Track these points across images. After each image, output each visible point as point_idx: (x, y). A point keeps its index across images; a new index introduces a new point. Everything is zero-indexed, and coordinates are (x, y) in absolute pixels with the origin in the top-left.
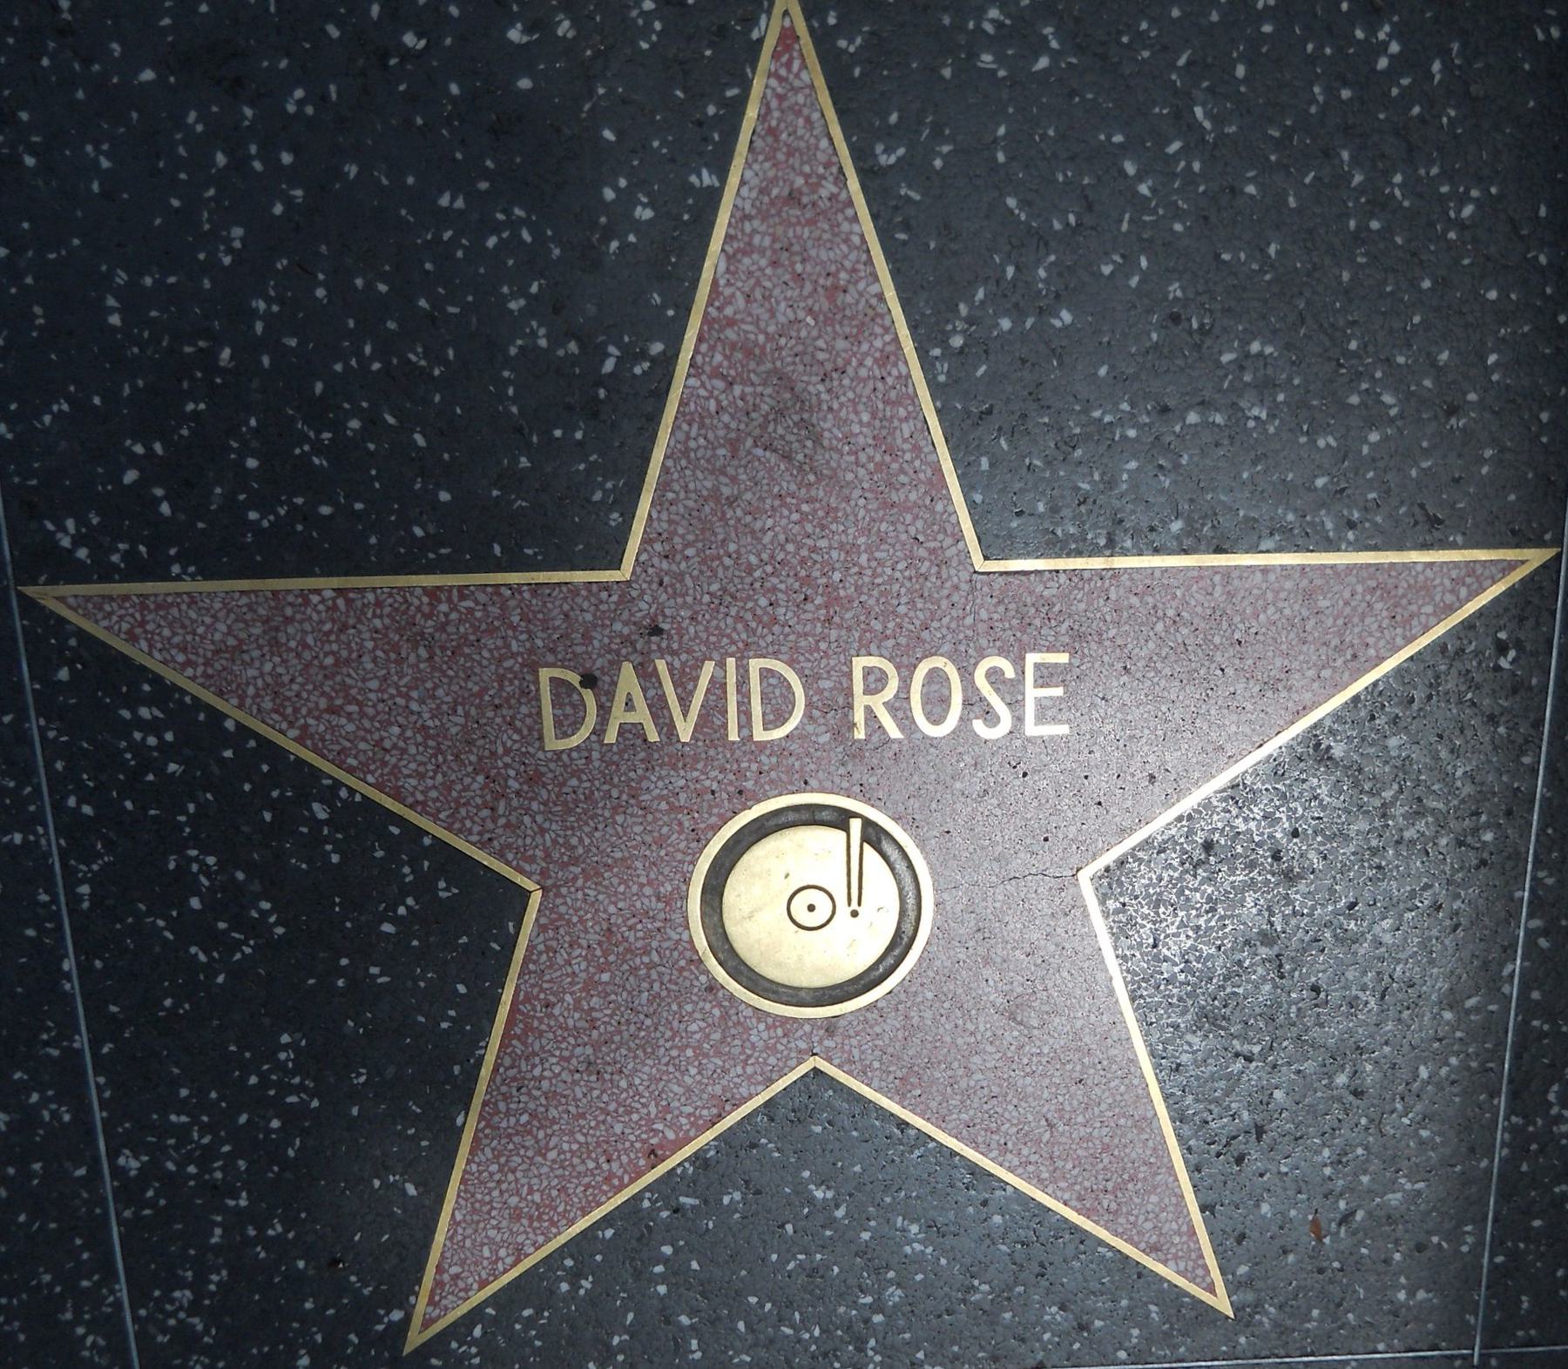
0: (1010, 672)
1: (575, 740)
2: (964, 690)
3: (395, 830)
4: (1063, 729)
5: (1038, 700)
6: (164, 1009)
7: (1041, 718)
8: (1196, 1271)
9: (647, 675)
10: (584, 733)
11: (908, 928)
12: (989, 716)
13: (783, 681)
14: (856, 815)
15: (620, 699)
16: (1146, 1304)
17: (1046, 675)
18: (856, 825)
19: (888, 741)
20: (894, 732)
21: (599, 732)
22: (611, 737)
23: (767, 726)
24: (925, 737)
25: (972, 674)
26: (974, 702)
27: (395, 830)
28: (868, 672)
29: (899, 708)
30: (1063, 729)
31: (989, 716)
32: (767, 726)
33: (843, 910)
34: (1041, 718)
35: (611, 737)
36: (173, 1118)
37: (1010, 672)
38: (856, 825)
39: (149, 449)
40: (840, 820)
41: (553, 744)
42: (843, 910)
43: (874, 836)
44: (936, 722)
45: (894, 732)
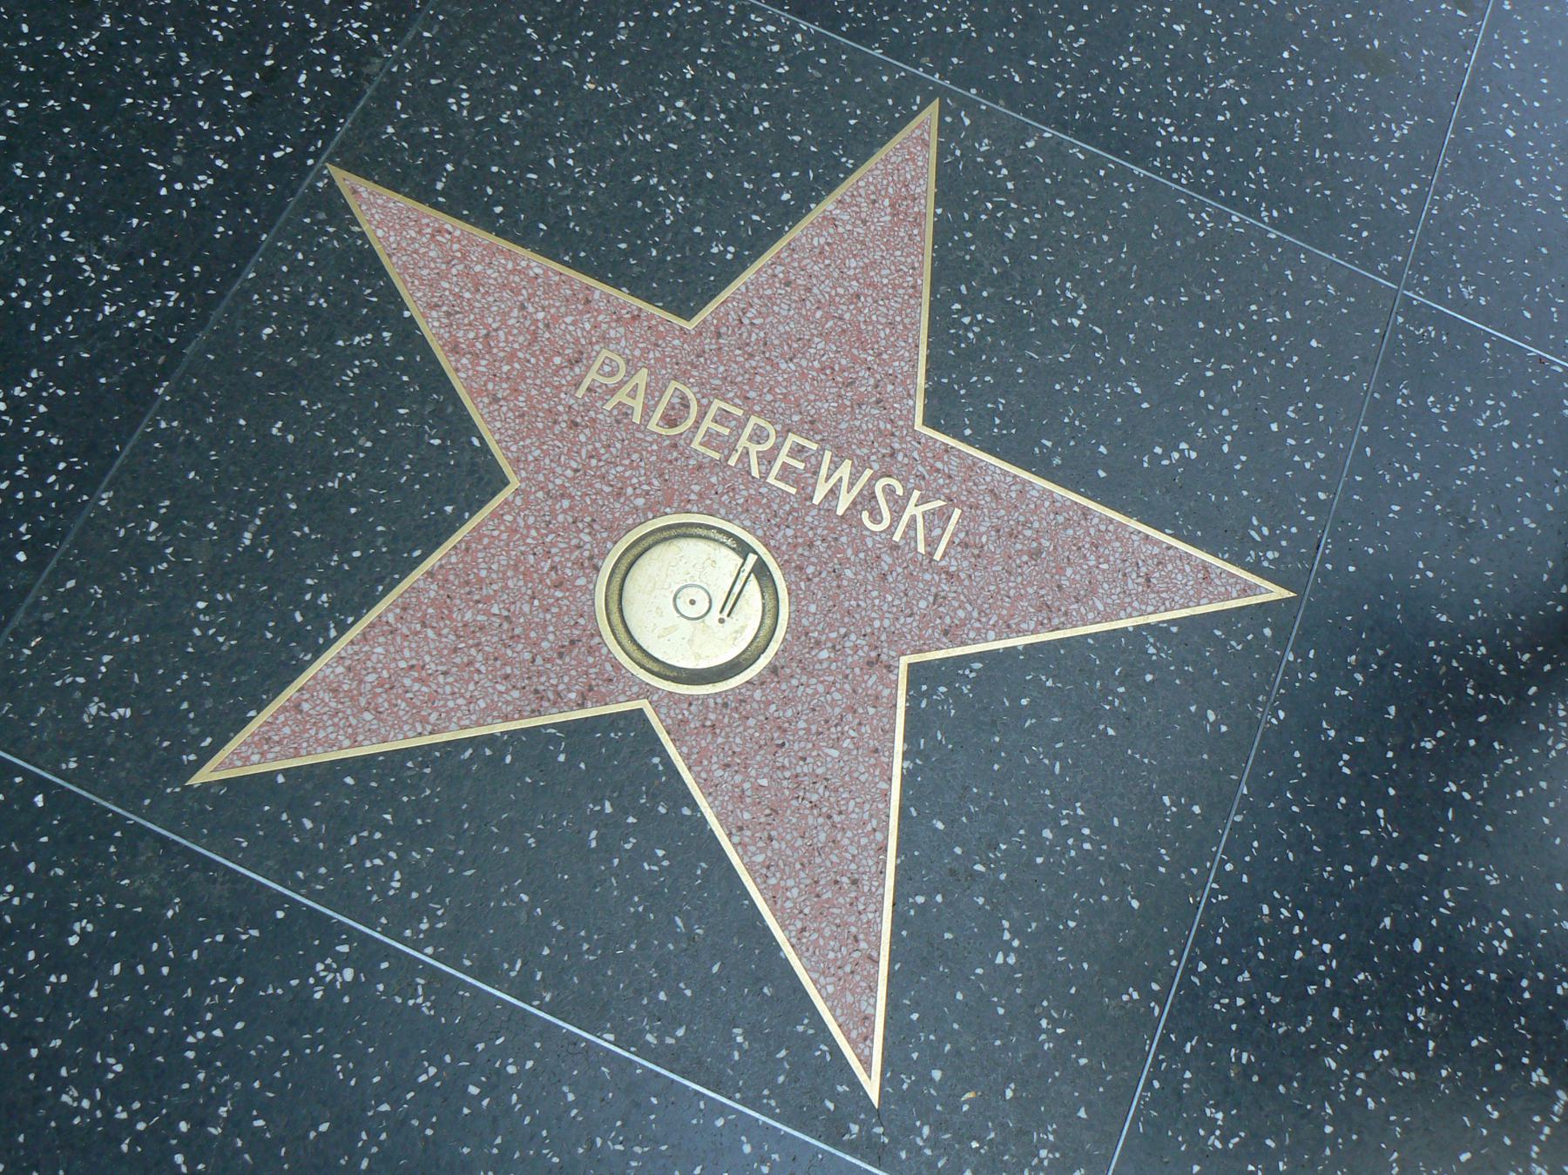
0: (900, 492)
7: (781, 477)
11: (761, 641)
12: (876, 516)
14: (755, 552)
15: (628, 388)
17: (798, 451)
18: (752, 559)
31: (876, 516)
33: (715, 614)
34: (781, 477)
36: (594, 834)
37: (900, 492)
38: (752, 559)
39: (1439, 336)
40: (743, 549)
42: (715, 614)
43: (761, 570)
44: (880, 522)
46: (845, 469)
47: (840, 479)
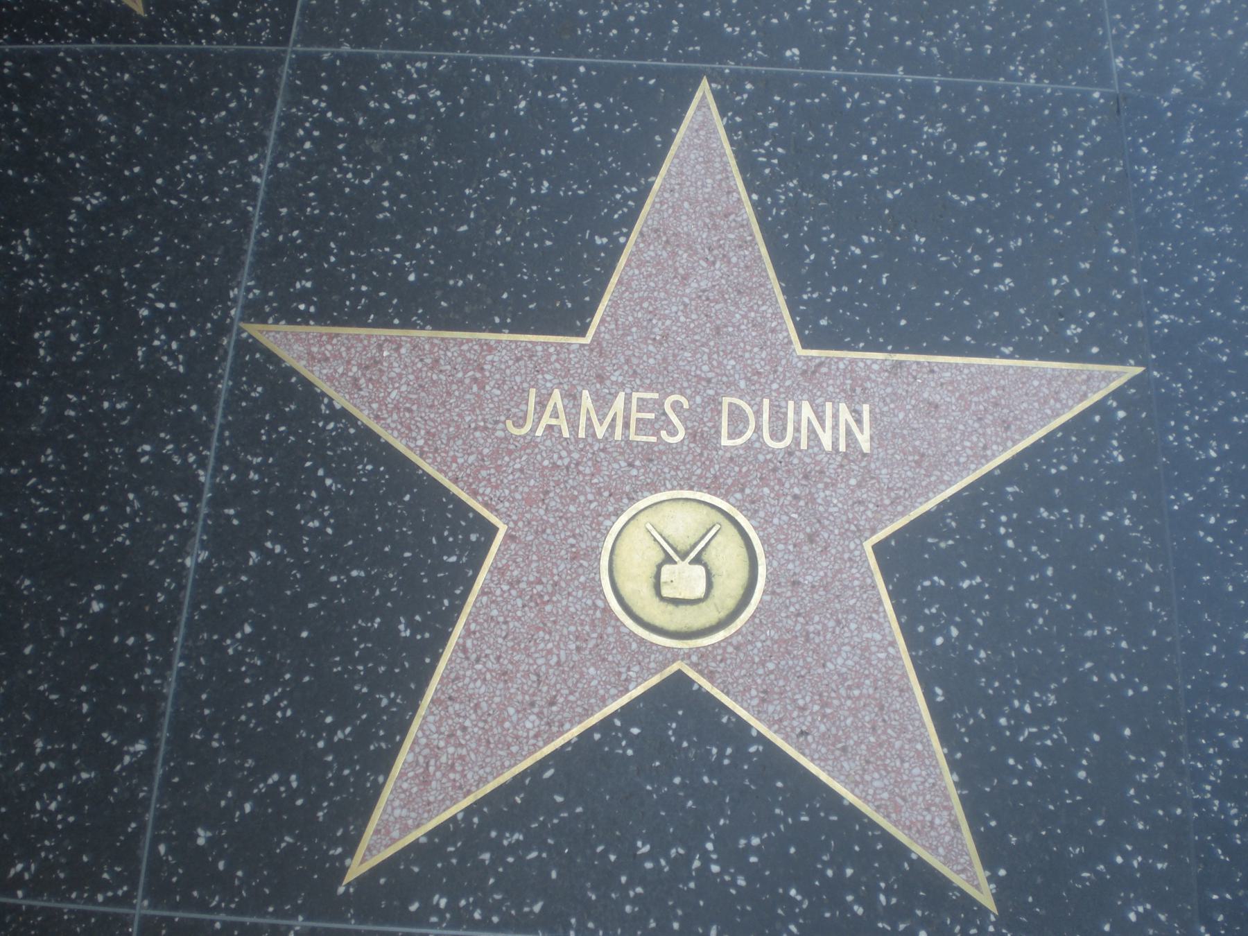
5: (638, 420)
6: (833, 915)
7: (638, 431)
8: (703, 104)
9: (572, 397)
10: (749, 434)
13: (738, 407)
15: (549, 409)
16: (1129, 252)
17: (643, 405)
21: (533, 430)
22: (539, 433)
23: (730, 437)
32: (730, 437)
34: (638, 431)
35: (539, 433)
41: (725, 441)
47: (589, 419)
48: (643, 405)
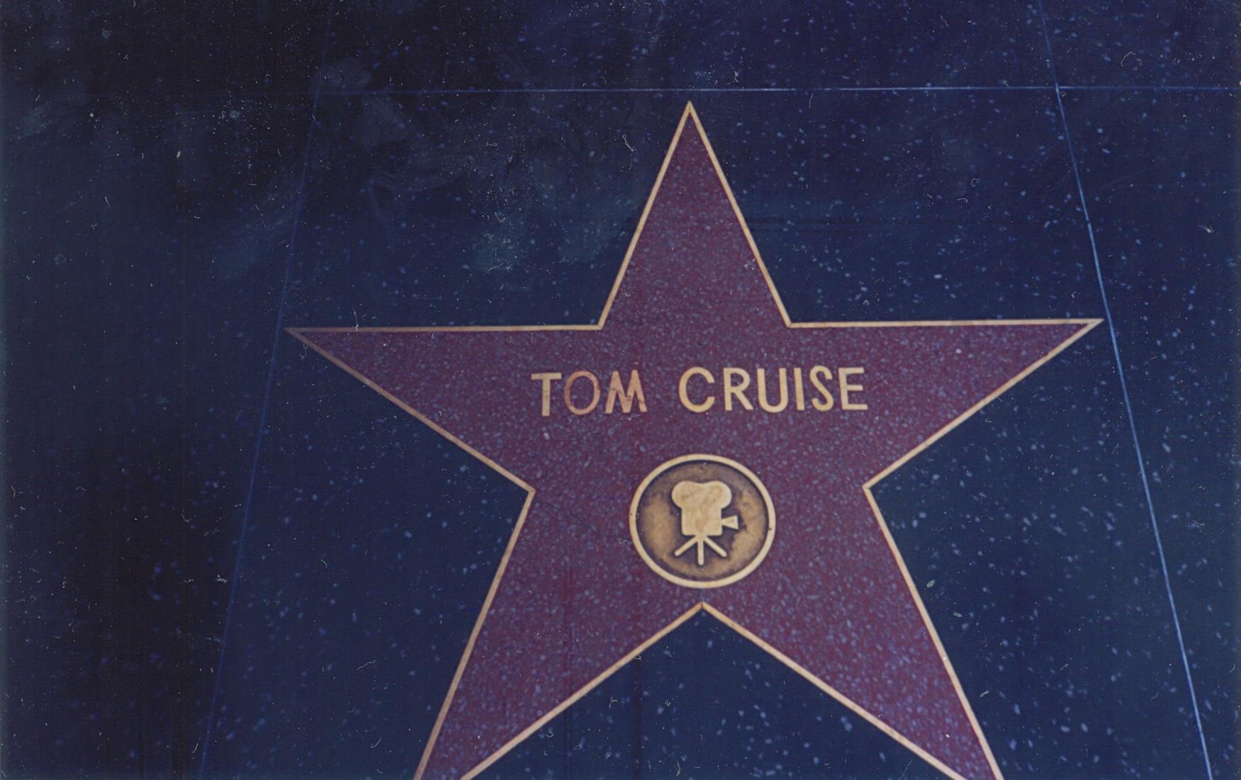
1: (572, 409)
2: (599, 403)
3: (499, 541)
4: (865, 407)
7: (851, 401)
17: (852, 379)
19: (745, 411)
20: (748, 406)
24: (783, 412)
25: (809, 372)
26: (810, 391)
27: (499, 541)
28: (733, 376)
29: (751, 393)
30: (865, 407)
34: (851, 401)
45: (748, 406)
46: (627, 408)
48: (852, 379)
